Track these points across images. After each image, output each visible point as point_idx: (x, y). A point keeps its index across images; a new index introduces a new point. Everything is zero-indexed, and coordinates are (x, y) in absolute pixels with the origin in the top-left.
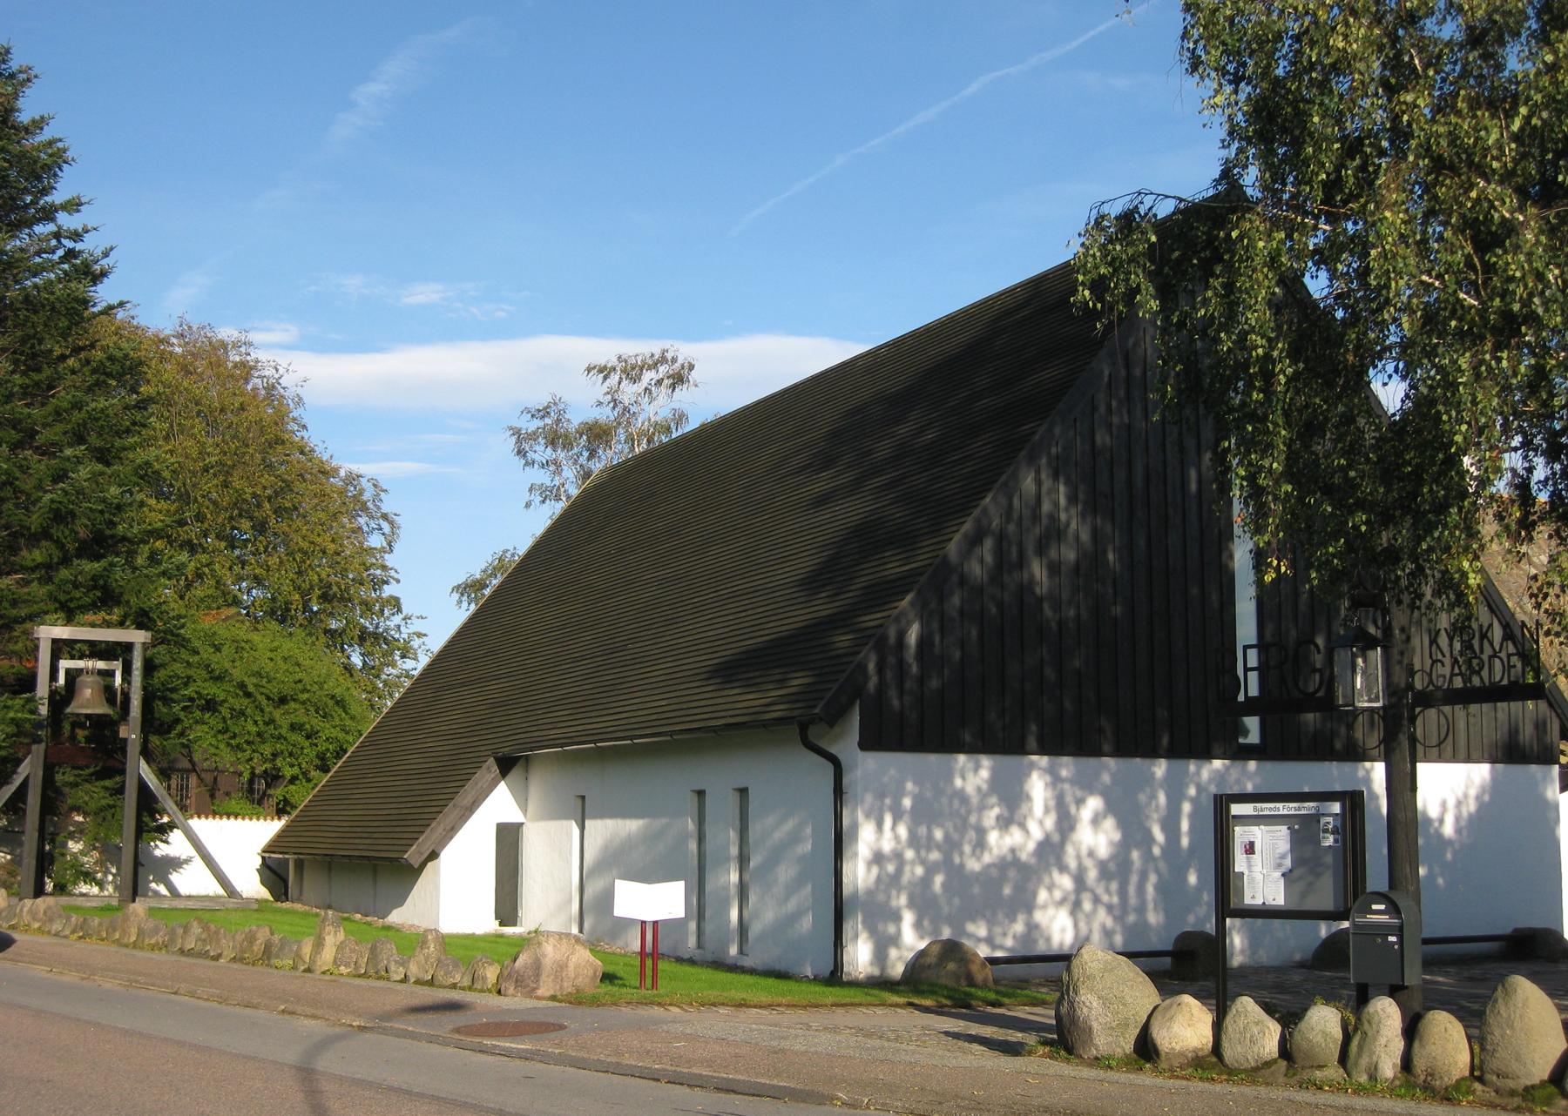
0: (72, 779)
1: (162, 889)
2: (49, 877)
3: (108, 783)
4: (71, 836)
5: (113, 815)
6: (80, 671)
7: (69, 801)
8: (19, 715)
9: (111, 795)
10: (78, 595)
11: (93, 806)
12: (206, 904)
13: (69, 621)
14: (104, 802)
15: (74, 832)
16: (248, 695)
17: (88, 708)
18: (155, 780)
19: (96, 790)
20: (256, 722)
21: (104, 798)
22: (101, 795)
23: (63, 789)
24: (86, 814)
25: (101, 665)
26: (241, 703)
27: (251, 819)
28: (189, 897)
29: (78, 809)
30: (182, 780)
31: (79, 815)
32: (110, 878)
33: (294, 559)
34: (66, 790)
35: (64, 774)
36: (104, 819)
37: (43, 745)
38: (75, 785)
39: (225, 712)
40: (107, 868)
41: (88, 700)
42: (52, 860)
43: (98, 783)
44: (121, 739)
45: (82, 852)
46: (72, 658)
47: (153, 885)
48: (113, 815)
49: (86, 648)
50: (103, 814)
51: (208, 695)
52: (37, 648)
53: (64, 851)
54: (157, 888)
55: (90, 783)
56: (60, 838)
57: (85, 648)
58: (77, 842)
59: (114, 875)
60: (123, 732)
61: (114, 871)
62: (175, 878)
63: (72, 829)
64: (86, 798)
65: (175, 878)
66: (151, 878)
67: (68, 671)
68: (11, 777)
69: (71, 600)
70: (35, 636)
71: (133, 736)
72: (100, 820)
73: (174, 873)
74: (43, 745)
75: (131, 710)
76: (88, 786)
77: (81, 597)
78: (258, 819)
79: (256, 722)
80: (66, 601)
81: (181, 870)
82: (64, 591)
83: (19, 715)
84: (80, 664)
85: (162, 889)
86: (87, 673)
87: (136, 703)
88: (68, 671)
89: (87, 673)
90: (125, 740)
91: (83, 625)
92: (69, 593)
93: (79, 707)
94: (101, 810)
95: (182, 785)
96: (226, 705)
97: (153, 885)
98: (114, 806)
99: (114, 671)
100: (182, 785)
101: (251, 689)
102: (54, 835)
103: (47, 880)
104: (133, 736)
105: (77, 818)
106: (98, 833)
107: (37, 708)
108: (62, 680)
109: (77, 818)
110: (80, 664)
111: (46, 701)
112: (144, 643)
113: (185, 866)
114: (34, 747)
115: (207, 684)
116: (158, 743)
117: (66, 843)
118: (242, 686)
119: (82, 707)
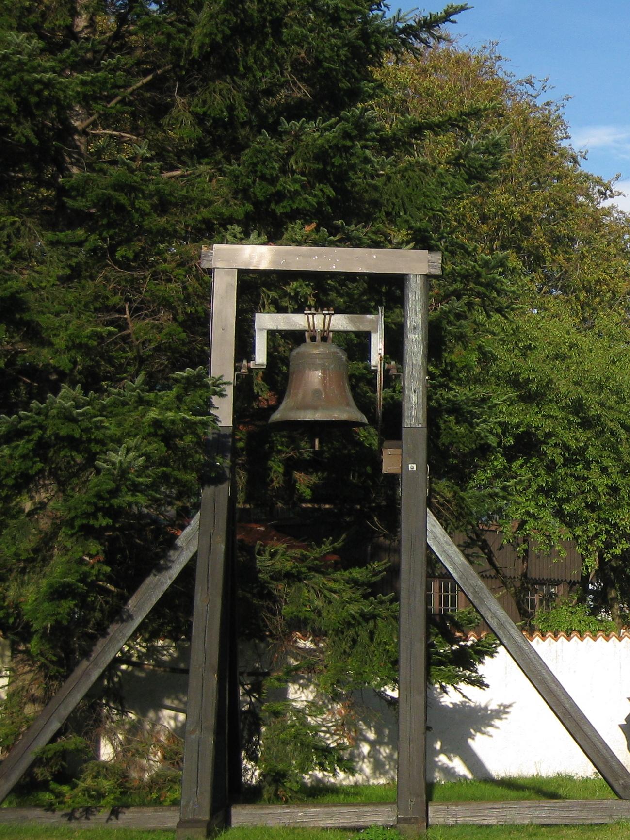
0: (289, 565)
1: (459, 766)
2: (253, 757)
3: (357, 573)
4: (293, 675)
5: (371, 635)
6: (296, 337)
7: (286, 609)
8: (170, 415)
9: (365, 596)
10: (292, 187)
11: (331, 617)
12: (575, 813)
13: (273, 239)
14: (353, 609)
15: (297, 668)
16: (586, 424)
17: (315, 408)
18: (460, 559)
19: (334, 586)
20: (604, 470)
21: (351, 601)
22: (346, 596)
23: (273, 585)
24: (318, 634)
25: (340, 322)
26: (574, 438)
27: (595, 638)
28: (510, 785)
29: (299, 624)
30: (446, 590)
31: (305, 638)
32: (365, 749)
33: (577, 299)
34: (280, 588)
35: (273, 555)
36: (354, 642)
37: (225, 489)
38: (292, 577)
39: (551, 452)
40: (359, 732)
41: (317, 392)
42: (254, 721)
43: (337, 575)
44: (387, 476)
45: (314, 707)
46: (281, 310)
47: (442, 759)
48: (371, 635)
49: (308, 291)
50: (351, 632)
51: (518, 426)
52: (206, 293)
53: (278, 706)
54: (451, 765)
55: (323, 573)
56: (269, 683)
57: (307, 290)
58: (304, 686)
59: (372, 744)
60: (390, 463)
61: (372, 736)
62: (479, 744)
63: (293, 662)
64: (318, 603)
65: (479, 744)
66: (438, 746)
67: (272, 334)
68: (164, 556)
69: (279, 197)
70: (205, 265)
71: (412, 467)
72: (345, 646)
73: (478, 736)
74: (225, 489)
75: (406, 413)
76: (319, 579)
77: (297, 192)
78: (607, 638)
79: (604, 470)
80: (268, 201)
81: (490, 729)
82: (263, 178)
83: (170, 415)
84: (298, 321)
85: (459, 766)
86: (313, 339)
87: (414, 398)
88: (272, 334)
89: (313, 339)
90: (393, 480)
91: (299, 244)
92: (273, 181)
93: (292, 409)
94: (349, 624)
95: (446, 597)
96: (553, 441)
97: (442, 759)
98: (374, 617)
99: (367, 335)
100: (446, 597)
101: (594, 410)
102: (259, 676)
103: (247, 764)
104: (412, 467)
105: (301, 643)
106: (343, 670)
107: (209, 404)
108: (261, 357)
109: (301, 643)
110: (298, 321)
111: (230, 391)
112: (428, 277)
113: (496, 722)
114: (207, 492)
115: (516, 409)
116: (449, 495)
117: (285, 691)
118: (578, 407)
119: (305, 407)
